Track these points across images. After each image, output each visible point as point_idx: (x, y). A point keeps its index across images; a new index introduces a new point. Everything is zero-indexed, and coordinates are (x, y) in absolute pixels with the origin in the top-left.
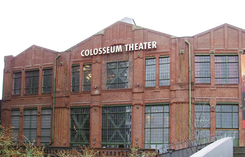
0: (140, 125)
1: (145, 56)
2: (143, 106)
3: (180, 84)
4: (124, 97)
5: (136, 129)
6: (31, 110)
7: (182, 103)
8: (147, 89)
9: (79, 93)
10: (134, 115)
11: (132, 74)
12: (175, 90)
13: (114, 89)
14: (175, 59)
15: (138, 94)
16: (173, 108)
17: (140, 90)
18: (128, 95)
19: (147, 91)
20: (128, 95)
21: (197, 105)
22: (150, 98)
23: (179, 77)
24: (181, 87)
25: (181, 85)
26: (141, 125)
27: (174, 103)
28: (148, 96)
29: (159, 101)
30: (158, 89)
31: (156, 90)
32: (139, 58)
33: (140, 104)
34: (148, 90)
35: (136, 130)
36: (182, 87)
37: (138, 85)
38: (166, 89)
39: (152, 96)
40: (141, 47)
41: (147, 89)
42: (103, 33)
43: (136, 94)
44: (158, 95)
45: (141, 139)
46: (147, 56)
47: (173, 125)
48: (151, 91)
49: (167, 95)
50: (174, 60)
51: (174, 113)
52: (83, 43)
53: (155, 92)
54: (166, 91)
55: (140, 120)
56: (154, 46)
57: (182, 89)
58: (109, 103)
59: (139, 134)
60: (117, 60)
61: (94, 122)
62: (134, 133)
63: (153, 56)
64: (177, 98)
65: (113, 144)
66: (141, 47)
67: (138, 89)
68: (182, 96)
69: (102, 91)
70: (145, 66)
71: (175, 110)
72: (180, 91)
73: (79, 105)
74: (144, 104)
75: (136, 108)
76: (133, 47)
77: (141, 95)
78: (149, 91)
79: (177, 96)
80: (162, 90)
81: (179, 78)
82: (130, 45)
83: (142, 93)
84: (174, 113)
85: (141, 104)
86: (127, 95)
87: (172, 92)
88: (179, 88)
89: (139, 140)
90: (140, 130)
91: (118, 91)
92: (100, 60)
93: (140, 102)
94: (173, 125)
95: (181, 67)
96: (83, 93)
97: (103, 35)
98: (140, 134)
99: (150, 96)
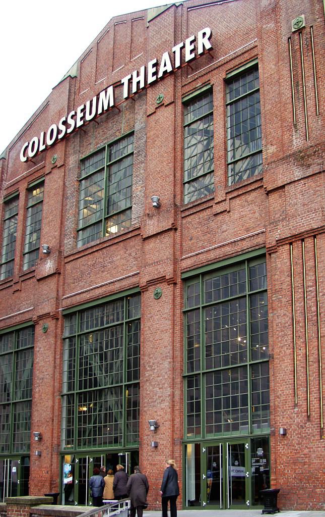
0: (166, 364)
1: (179, 94)
2: (175, 284)
3: (300, 152)
4: (124, 261)
5: (153, 383)
6: (18, 331)
7: (291, 244)
8: (187, 213)
9: (15, 281)
10: (147, 328)
11: (142, 172)
12: (283, 187)
13: (93, 244)
14: (275, 65)
15: (158, 241)
16: (279, 266)
17: (164, 224)
18: (133, 254)
19: (189, 219)
20: (133, 254)
21: (43, 281)
22: (200, 244)
23: (295, 126)
24: (302, 165)
25: (303, 158)
26: (170, 362)
27: (281, 242)
28: (191, 239)
29: (228, 250)
30: (225, 200)
31: (218, 209)
32: (161, 109)
33: (162, 280)
34: (192, 217)
35: (154, 386)
36: (309, 166)
37: (155, 204)
38: (254, 194)
39: (205, 233)
40: (165, 65)
41: (187, 213)
42: (73, 74)
43: (153, 240)
44: (224, 227)
45: (168, 424)
46: (187, 89)
47: (282, 347)
48: (201, 215)
49: (257, 215)
50: (273, 67)
51: (284, 286)
52: (31, 124)
53: (213, 218)
54: (253, 202)
55: (166, 344)
56: (204, 43)
57: (310, 172)
58: (81, 295)
59: (163, 406)
60: (105, 139)
61: (41, 376)
62: (146, 400)
63: (204, 84)
64: (293, 216)
65: (247, 342)
66: (165, 65)
67: (158, 221)
68: (312, 202)
69: (63, 259)
70: (179, 129)
71: (286, 274)
72: (300, 186)
73: (14, 321)
74: (179, 274)
75: (153, 296)
76: (141, 78)
77: (167, 239)
78: (195, 219)
79: (291, 211)
80: (237, 201)
81: (296, 131)
82: (135, 74)
83: (171, 233)
84: (284, 286)
85: (167, 277)
86: (130, 255)
87: (274, 197)
88: (298, 173)
89: (162, 428)
90: (166, 385)
91: (105, 246)
92: (61, 158)
93: (162, 270)
94: (282, 347)
95: (297, 86)
96: (22, 279)
97: (76, 77)
98: (166, 404)
99: (198, 238)
